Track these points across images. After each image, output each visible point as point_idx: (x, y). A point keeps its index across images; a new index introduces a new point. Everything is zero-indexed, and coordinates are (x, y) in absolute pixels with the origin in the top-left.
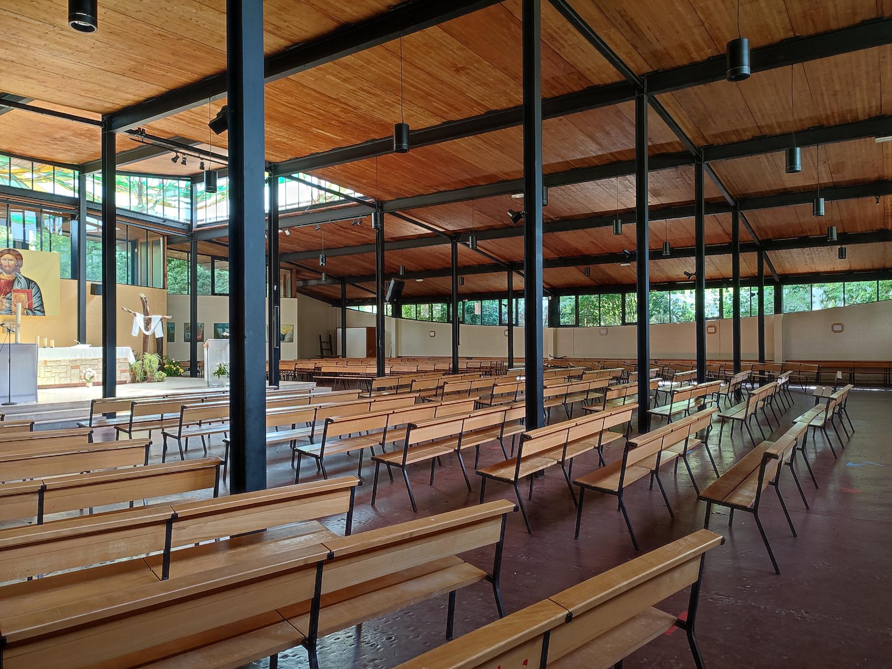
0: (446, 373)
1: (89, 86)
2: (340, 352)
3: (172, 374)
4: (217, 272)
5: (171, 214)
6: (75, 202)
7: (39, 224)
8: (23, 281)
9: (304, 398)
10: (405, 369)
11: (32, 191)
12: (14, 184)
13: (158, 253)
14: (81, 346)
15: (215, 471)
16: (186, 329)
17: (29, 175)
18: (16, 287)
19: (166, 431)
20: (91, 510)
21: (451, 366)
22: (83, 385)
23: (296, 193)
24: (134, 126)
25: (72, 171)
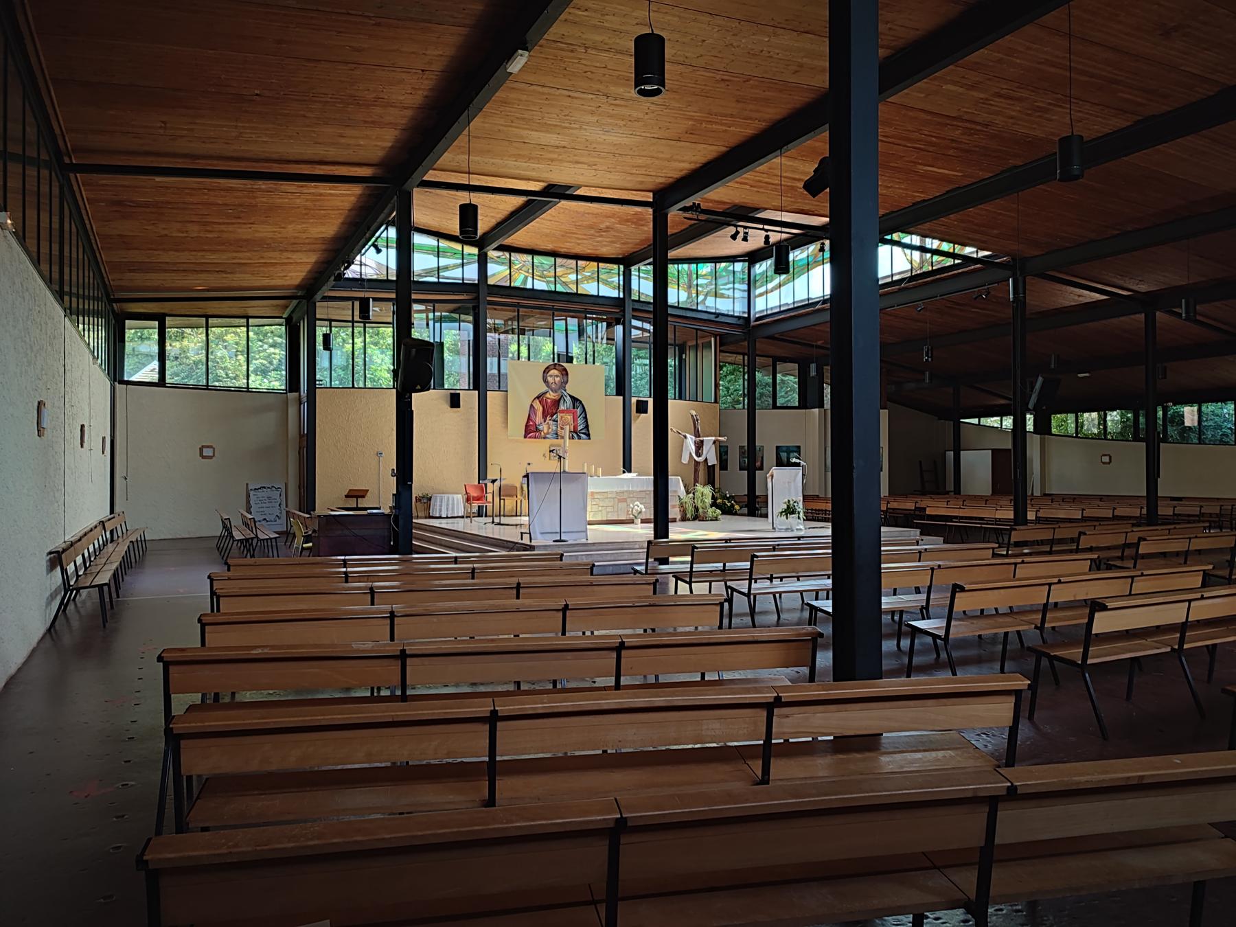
0: (1137, 522)
1: (640, 161)
2: (950, 486)
3: (728, 511)
4: (779, 376)
5: (724, 306)
6: (618, 303)
7: (581, 332)
8: (568, 399)
9: (910, 552)
10: (1061, 514)
11: (577, 294)
12: (560, 288)
13: (709, 358)
14: (627, 475)
15: (810, 645)
16: (742, 454)
17: (573, 277)
18: (562, 407)
19: (729, 583)
20: (657, 677)
21: (1144, 511)
22: (632, 522)
23: (893, 261)
24: (688, 202)
25: (616, 266)
